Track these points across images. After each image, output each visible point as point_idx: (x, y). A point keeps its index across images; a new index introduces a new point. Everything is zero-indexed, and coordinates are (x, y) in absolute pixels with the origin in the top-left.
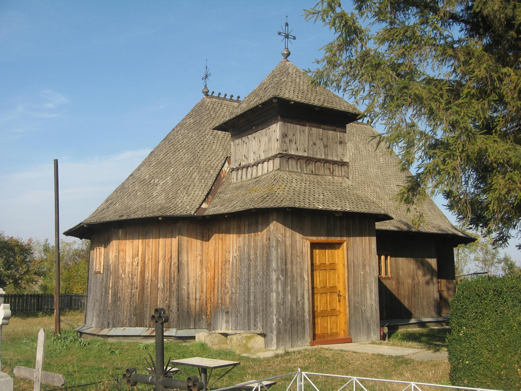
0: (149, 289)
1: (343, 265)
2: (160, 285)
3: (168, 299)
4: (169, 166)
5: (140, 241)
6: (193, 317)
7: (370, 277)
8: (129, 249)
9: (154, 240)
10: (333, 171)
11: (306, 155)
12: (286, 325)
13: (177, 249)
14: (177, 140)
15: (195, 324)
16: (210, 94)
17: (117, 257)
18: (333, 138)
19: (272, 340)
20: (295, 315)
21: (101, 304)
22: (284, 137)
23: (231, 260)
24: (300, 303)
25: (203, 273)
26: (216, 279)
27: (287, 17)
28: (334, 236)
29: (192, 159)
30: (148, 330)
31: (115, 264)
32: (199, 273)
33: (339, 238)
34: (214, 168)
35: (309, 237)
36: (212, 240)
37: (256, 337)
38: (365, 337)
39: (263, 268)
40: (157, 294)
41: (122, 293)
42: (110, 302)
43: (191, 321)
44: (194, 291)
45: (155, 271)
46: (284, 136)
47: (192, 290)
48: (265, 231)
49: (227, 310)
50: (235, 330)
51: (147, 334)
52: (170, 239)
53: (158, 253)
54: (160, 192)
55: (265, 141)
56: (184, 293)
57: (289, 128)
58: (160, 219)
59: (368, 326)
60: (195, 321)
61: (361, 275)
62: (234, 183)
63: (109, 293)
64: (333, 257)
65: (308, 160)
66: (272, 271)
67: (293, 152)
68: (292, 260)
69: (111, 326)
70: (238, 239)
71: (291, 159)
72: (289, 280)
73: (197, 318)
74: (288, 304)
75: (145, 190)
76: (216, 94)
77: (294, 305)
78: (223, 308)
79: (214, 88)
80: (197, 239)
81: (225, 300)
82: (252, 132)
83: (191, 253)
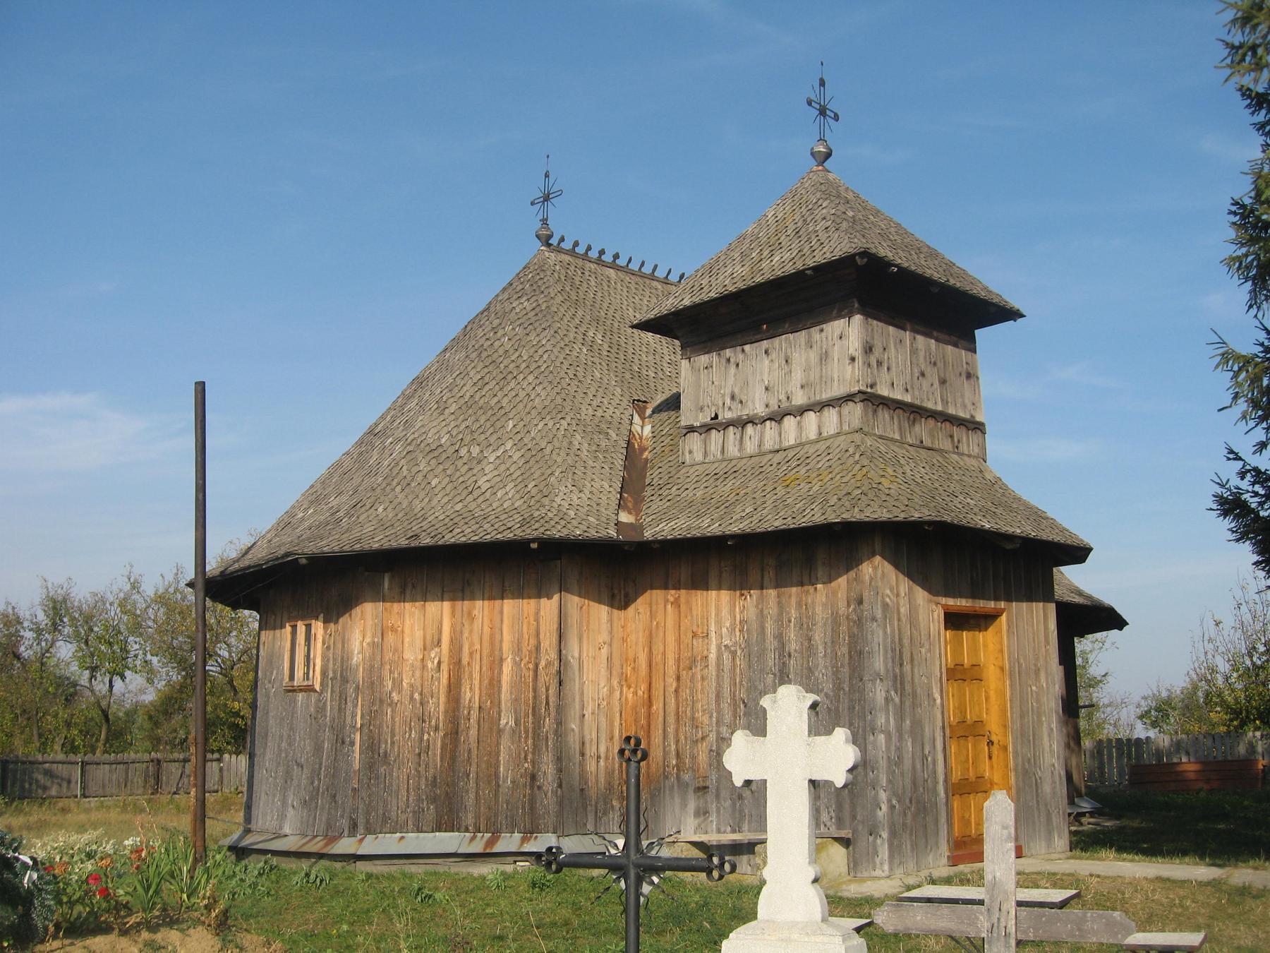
0: (473, 732)
1: (998, 671)
2: (507, 720)
3: (530, 757)
4: (498, 415)
5: (447, 605)
6: (593, 803)
7: (1048, 700)
8: (412, 625)
9: (486, 602)
10: (959, 441)
11: (908, 398)
12: (905, 814)
13: (556, 626)
14: (501, 351)
15: (596, 821)
16: (554, 241)
17: (378, 647)
18: (955, 364)
19: (876, 853)
20: (921, 789)
21: (315, 774)
22: (866, 352)
23: (713, 656)
24: (929, 759)
25: (614, 690)
26: (657, 706)
27: (822, 64)
28: (983, 598)
29: (559, 400)
30: (473, 839)
31: (372, 666)
32: (605, 689)
33: (992, 604)
34: (615, 423)
35: (943, 600)
36: (641, 605)
37: (830, 846)
38: (1043, 844)
39: (836, 673)
40: (498, 744)
41: (393, 743)
42: (356, 766)
43: (589, 814)
44: (594, 735)
45: (491, 683)
46: (868, 349)
47: (590, 735)
48: (842, 581)
49: (702, 784)
50: (734, 831)
51: (477, 847)
52: (533, 601)
53: (498, 636)
54: (498, 479)
55: (807, 360)
56: (573, 741)
57: (875, 330)
58: (534, 546)
59: (1049, 815)
60: (596, 812)
61: (1032, 694)
62: (692, 462)
63: (352, 743)
64: (974, 650)
65: (915, 412)
66: (873, 681)
67: (883, 391)
68: (912, 654)
69: (361, 829)
70: (739, 603)
71: (826, 409)
72: (907, 704)
73: (601, 805)
74: (907, 763)
75: (449, 472)
76: (567, 245)
77: (919, 766)
78: (686, 777)
79: (564, 226)
80: (600, 602)
81: (693, 758)
82: (758, 337)
83: (588, 638)
